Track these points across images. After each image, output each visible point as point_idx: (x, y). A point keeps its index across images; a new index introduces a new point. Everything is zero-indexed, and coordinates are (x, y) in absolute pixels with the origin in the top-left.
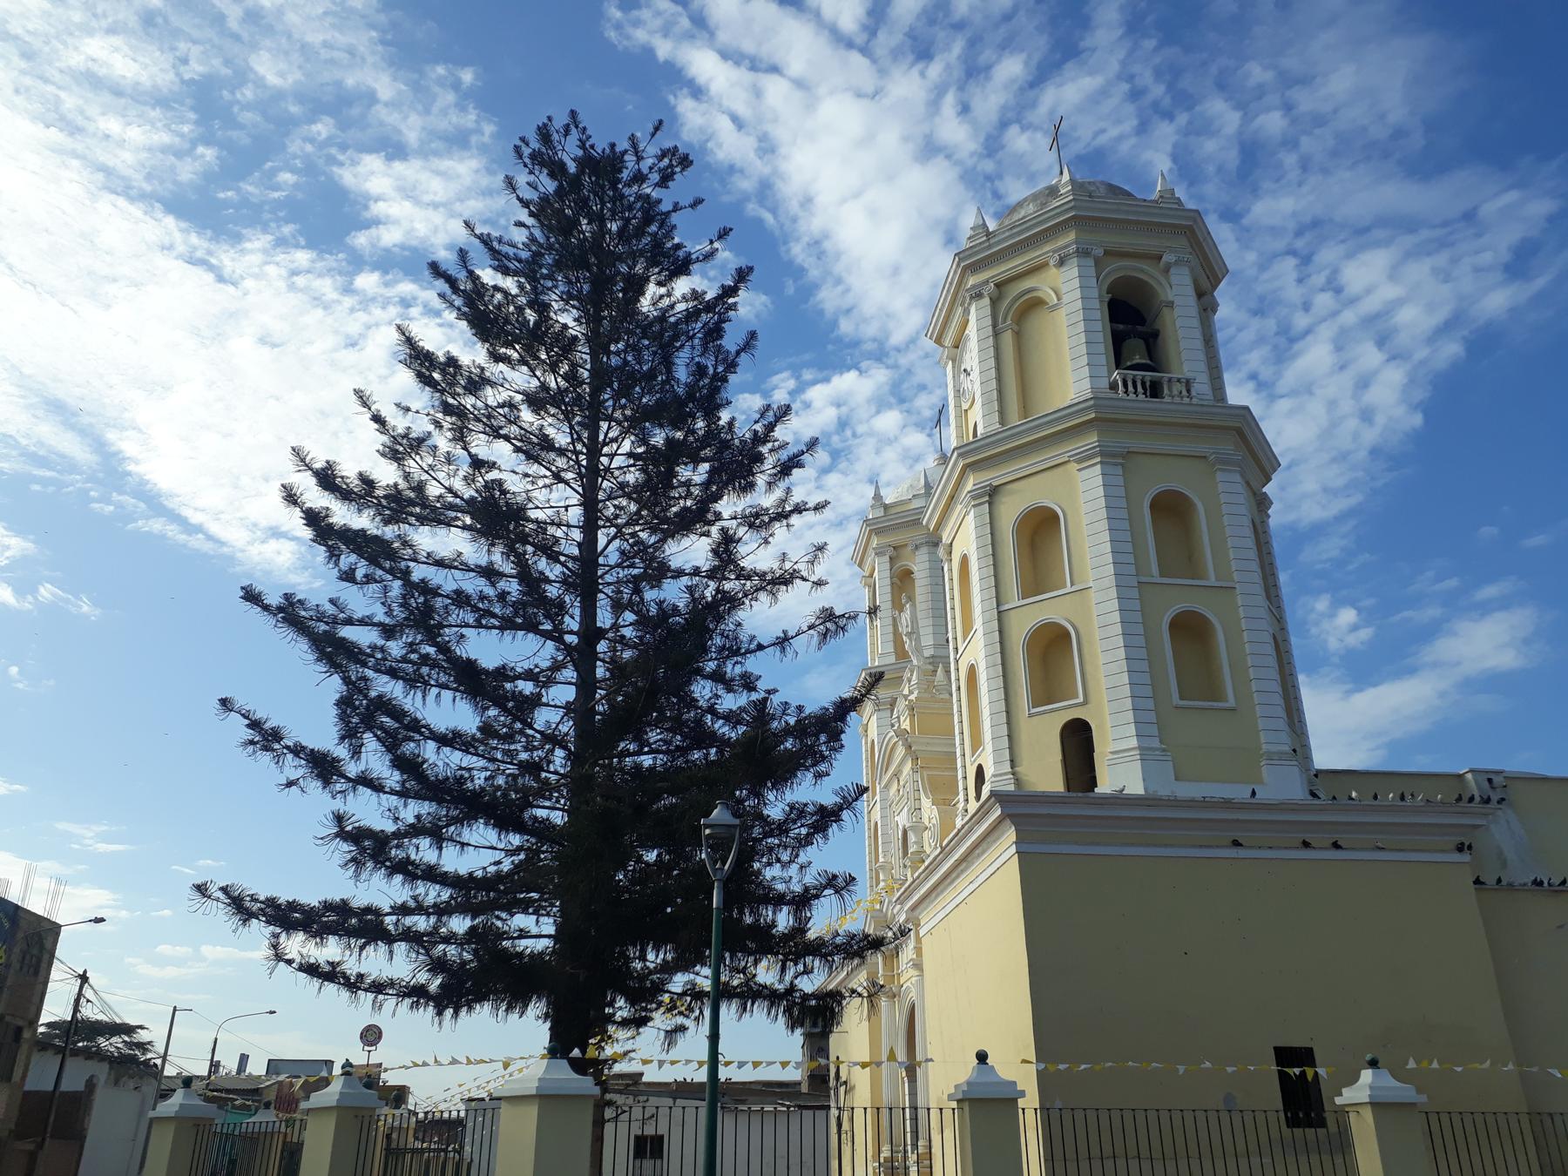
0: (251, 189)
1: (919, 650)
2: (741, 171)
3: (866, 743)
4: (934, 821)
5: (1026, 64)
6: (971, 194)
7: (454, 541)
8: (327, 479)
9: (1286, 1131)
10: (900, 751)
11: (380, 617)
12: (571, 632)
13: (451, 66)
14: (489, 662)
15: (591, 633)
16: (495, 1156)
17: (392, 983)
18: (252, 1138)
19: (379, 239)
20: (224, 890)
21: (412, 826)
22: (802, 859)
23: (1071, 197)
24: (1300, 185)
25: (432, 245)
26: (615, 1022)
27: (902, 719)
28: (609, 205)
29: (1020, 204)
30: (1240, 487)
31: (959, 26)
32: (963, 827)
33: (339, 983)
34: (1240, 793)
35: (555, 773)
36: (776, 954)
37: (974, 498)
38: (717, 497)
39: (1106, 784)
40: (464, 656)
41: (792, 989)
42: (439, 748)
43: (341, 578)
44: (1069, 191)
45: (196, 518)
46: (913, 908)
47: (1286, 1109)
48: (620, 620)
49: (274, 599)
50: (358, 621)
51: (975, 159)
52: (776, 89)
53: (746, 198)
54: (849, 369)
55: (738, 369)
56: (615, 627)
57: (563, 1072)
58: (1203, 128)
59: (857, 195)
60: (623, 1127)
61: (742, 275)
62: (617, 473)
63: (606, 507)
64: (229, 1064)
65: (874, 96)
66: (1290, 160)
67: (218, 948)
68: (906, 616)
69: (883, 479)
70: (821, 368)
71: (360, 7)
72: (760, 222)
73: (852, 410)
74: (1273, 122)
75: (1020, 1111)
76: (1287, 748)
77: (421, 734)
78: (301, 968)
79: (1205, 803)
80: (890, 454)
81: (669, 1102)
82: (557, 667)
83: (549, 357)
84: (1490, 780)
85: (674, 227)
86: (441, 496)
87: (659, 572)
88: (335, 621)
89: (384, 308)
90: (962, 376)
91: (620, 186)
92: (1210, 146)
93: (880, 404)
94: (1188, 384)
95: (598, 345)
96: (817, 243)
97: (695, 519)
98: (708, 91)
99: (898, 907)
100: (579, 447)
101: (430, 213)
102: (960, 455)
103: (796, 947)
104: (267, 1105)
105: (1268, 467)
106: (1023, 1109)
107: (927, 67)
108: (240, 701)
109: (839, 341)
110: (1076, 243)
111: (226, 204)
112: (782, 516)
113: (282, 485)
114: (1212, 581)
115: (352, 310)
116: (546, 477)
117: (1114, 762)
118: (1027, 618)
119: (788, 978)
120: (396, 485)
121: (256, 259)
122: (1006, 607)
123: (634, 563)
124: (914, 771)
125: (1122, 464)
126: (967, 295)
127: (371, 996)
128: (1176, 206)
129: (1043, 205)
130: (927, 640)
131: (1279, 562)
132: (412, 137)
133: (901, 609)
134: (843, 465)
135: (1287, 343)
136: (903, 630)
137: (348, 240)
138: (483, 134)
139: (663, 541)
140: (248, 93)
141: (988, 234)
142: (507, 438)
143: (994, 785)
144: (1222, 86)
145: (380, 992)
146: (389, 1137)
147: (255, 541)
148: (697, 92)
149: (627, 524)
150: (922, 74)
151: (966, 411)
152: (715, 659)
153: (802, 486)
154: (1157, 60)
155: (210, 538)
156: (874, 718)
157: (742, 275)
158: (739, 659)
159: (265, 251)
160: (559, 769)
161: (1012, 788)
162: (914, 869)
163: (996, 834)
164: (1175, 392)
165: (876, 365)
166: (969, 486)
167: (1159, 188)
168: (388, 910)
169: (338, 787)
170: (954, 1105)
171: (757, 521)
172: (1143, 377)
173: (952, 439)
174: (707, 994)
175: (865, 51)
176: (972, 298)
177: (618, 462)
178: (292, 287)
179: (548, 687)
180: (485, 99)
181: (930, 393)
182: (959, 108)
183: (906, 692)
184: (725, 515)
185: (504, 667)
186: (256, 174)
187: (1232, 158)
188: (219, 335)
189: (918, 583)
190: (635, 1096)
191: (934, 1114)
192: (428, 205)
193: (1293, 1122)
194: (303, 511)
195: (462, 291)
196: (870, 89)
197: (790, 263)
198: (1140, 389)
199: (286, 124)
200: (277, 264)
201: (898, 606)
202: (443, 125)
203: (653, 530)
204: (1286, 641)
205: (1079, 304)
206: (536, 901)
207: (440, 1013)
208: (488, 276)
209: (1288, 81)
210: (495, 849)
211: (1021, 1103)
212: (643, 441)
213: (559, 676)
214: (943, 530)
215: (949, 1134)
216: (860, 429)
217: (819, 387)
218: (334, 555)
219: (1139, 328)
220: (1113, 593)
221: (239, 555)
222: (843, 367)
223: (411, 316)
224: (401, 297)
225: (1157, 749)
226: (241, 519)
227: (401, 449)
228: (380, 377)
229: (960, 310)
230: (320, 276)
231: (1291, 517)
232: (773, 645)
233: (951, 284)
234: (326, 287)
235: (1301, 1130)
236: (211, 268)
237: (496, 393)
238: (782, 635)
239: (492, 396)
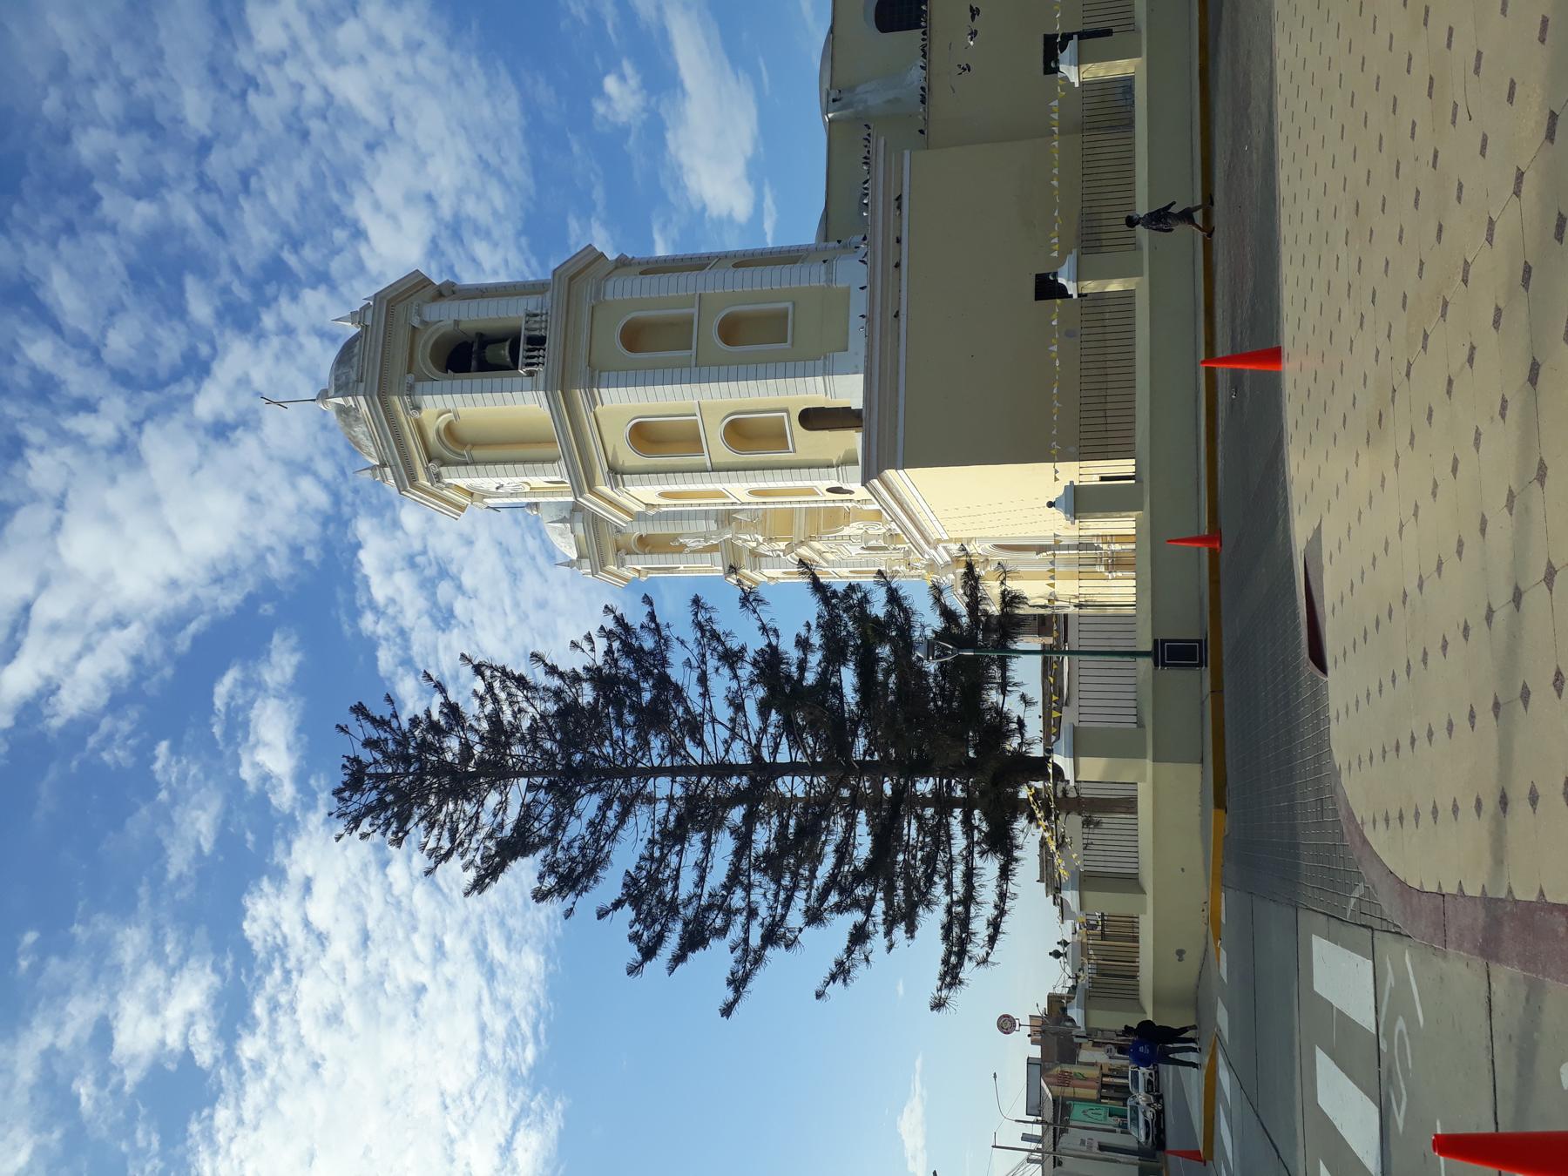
3: (784, 578)
4: (861, 526)
8: (649, 953)
27: (777, 548)
37: (617, 485)
39: (857, 403)
44: (353, 399)
46: (928, 543)
84: (834, 100)
88: (746, 951)
102: (581, 496)
108: (818, 985)
114: (695, 311)
118: (717, 449)
122: (709, 464)
125: (600, 372)
130: (702, 526)
156: (766, 572)
164: (537, 326)
169: (871, 928)
170: (1077, 521)
189: (651, 532)
191: (1082, 533)
198: (535, 353)
201: (681, 549)
204: (735, 254)
207: (1016, 860)
211: (1076, 483)
225: (825, 364)
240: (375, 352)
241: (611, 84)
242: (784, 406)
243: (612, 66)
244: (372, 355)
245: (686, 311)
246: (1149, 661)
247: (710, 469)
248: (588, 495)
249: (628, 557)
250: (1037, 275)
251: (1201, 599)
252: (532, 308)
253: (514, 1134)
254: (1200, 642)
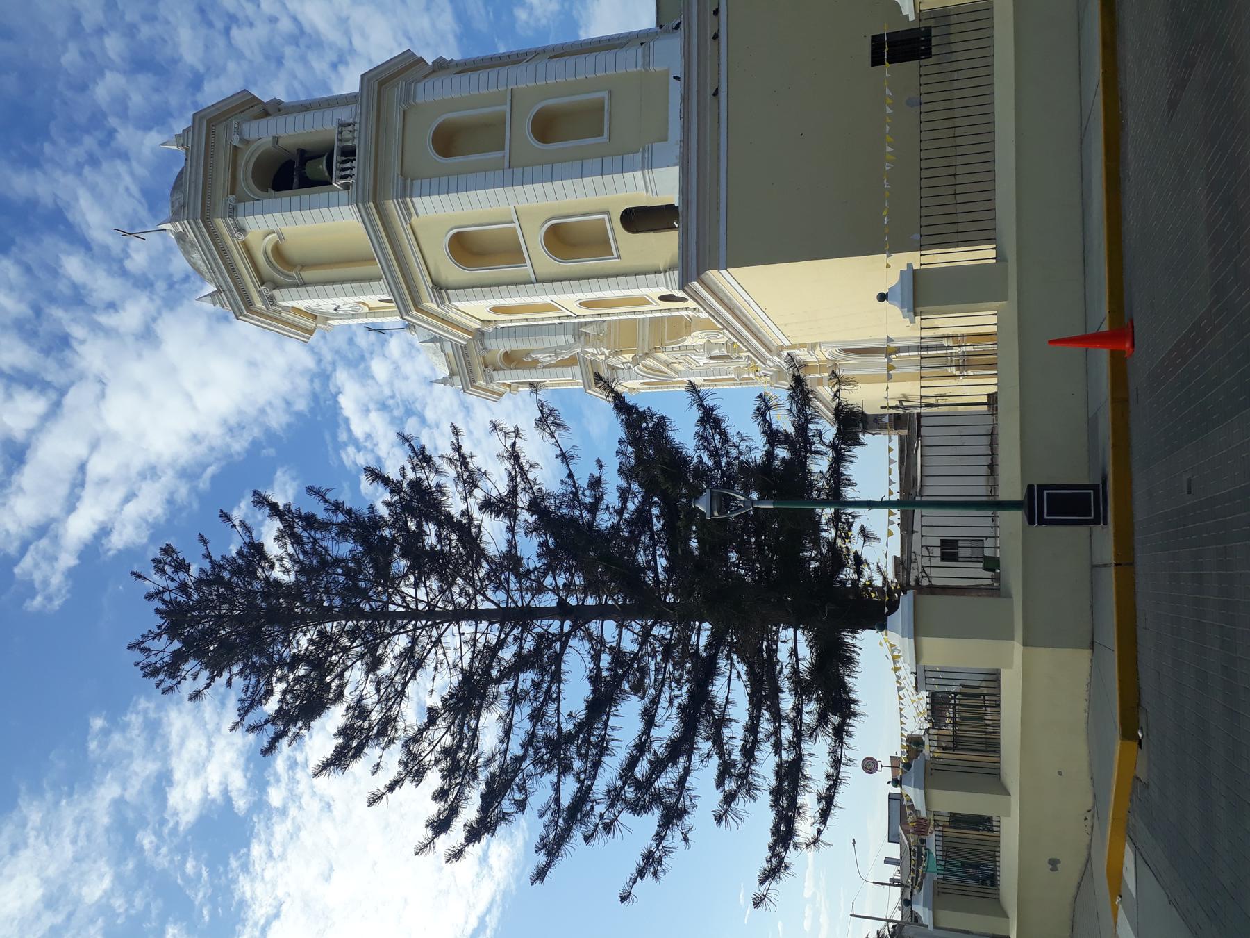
0: (201, 895)
1: (568, 347)
2: (172, 493)
3: (644, 389)
5: (69, 254)
6: (186, 302)
7: (489, 727)
8: (440, 826)
9: (933, 60)
10: (649, 362)
11: (553, 777)
12: (562, 626)
13: (89, 737)
14: (586, 690)
15: (563, 610)
16: (958, 668)
17: (833, 752)
18: (947, 852)
19: (239, 790)
20: (762, 883)
21: (714, 743)
22: (736, 439)
23: (186, 222)
24: (168, 22)
25: (244, 746)
26: (859, 580)
27: (624, 360)
28: (208, 611)
29: (193, 265)
30: (429, 83)
31: (38, 311)
32: (707, 312)
33: (834, 793)
34: (676, 90)
35: (671, 632)
36: (806, 458)
37: (443, 302)
38: (449, 516)
39: (674, 198)
40: (585, 712)
41: (833, 446)
42: (656, 726)
43: (523, 811)
44: (181, 224)
45: (473, 923)
46: (769, 350)
47: (919, 59)
48: (550, 587)
49: (542, 858)
50: (556, 794)
51: (155, 297)
52: (99, 466)
53: (194, 490)
54: (337, 402)
55: (340, 500)
56: (556, 590)
57: (897, 619)
58: (121, 105)
59: (189, 397)
60: (934, 572)
61: (260, 500)
62: (431, 596)
63: (459, 604)
64: (892, 871)
65: (104, 383)
66: (145, 31)
67: (806, 884)
68: (543, 358)
69: (427, 372)
70: (337, 425)
71: (41, 815)
72: (214, 478)
73: (372, 399)
74: (114, 45)
75: (923, 267)
76: (640, 50)
77: (646, 741)
78: (824, 823)
79: (685, 118)
80: (407, 368)
81: (916, 537)
82: (589, 636)
83: (337, 653)
85: (223, 557)
86: (452, 735)
87: (511, 560)
88: (557, 812)
89: (298, 782)
90: (341, 312)
91: (191, 603)
92: (136, 100)
93: (366, 376)
94: (342, 125)
95: (327, 615)
96: (231, 430)
97: (467, 532)
98: (103, 522)
99: (769, 363)
100: (410, 627)
101: (216, 749)
102: (407, 314)
103: (801, 442)
104: (923, 841)
105: (411, 60)
106: (921, 265)
107: (76, 338)
108: (621, 885)
109: (312, 410)
110: (224, 218)
111: (213, 914)
112: (463, 461)
113: (447, 862)
115: (300, 808)
116: (436, 653)
117: (654, 191)
118: (540, 259)
119: (823, 448)
120: (441, 771)
121: (259, 888)
123: (505, 579)
124: (665, 350)
125: (412, 180)
126: (271, 308)
127: (843, 768)
128: (190, 133)
129: (193, 245)
130: (561, 340)
131: (489, 53)
132: (152, 767)
133: (536, 361)
134: (418, 406)
135: (303, 37)
136: (553, 360)
137: (241, 814)
138: (148, 708)
139: (486, 557)
140: (119, 903)
141: (219, 291)
142: (405, 685)
143: (674, 287)
144: (82, 88)
145: (840, 761)
146: (944, 749)
147: (490, 875)
148: (104, 532)
149: (473, 586)
150: (83, 342)
151: (370, 309)
152: (581, 511)
153: (439, 444)
154: (62, 142)
155: (489, 911)
157: (260, 500)
158: (580, 492)
159: (253, 880)
160: (668, 630)
161: (676, 273)
162: (739, 350)
163: (714, 287)
164: (350, 136)
165: (333, 380)
166: (433, 306)
167: (175, 147)
168: (777, 759)
169: (687, 803)
170: (918, 318)
171: (470, 481)
172: (337, 162)
173: (395, 320)
174: (837, 511)
175: (62, 392)
176: (274, 305)
177: (422, 595)
178: (283, 857)
179: (605, 642)
180: (116, 710)
181: (355, 335)
182: (111, 311)
183: (603, 357)
184: (464, 507)
185: (590, 678)
186: (188, 892)
187: (146, 80)
188: (324, 914)
189: (515, 348)
190: (911, 562)
191: (925, 333)
192: (210, 751)
193: (928, 54)
194: (468, 844)
195: (285, 728)
196: (98, 387)
197: (248, 451)
198: (348, 165)
199: (144, 871)
200: (263, 870)
201: (534, 364)
202: (141, 741)
203: (478, 564)
205: (277, 215)
206: (768, 643)
207: (855, 715)
208: (272, 706)
209: (76, 28)
210: (730, 677)
211: (916, 266)
212: (405, 576)
213: (596, 633)
214: (470, 327)
215: (938, 322)
216: (387, 392)
217: (353, 427)
218: (503, 817)
219: (296, 165)
220: (519, 188)
221: (502, 887)
222: (336, 408)
223: (303, 760)
224: (289, 769)
225: (643, 158)
226: (473, 886)
227: (416, 768)
228: (355, 783)
229: (284, 314)
230: (272, 835)
231: (451, 39)
232: (568, 465)
233: (262, 322)
234: (281, 830)
235: (933, 48)
236: (268, 923)
237: (368, 696)
238: (560, 458)
239: (371, 698)
240: (197, 174)
242: (603, 207)
244: (193, 178)
245: (498, 108)
247: (534, 279)
249: (495, 373)
250: (872, 37)
251: (1092, 423)
252: (346, 118)
253: (488, 848)
254: (1095, 488)
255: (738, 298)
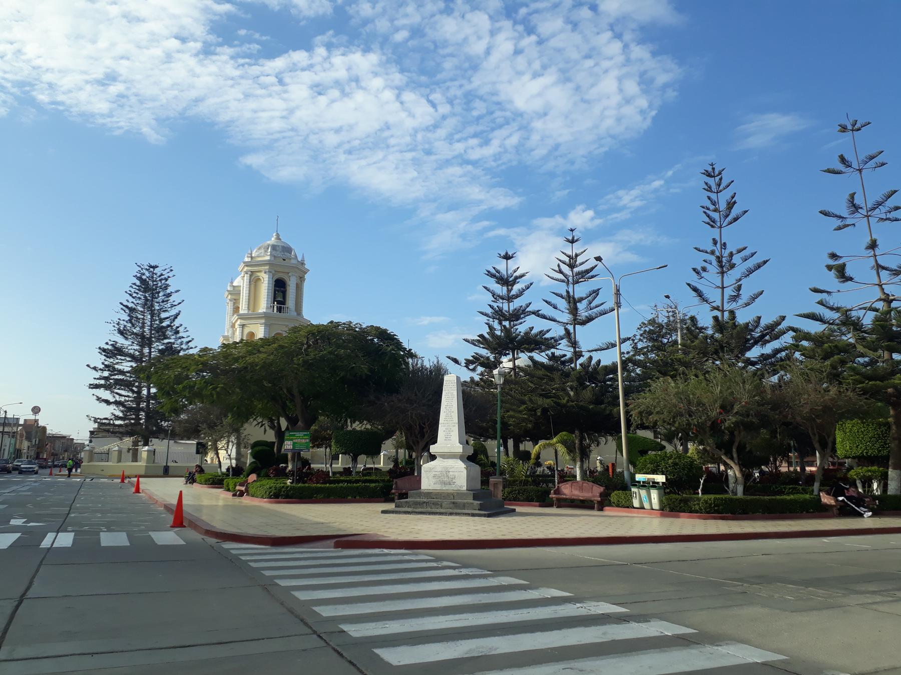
108: (95, 394)
241: (590, 213)
243: (598, 214)
246: (165, 465)
248: (237, 317)
249: (232, 303)
255: (54, 533)
